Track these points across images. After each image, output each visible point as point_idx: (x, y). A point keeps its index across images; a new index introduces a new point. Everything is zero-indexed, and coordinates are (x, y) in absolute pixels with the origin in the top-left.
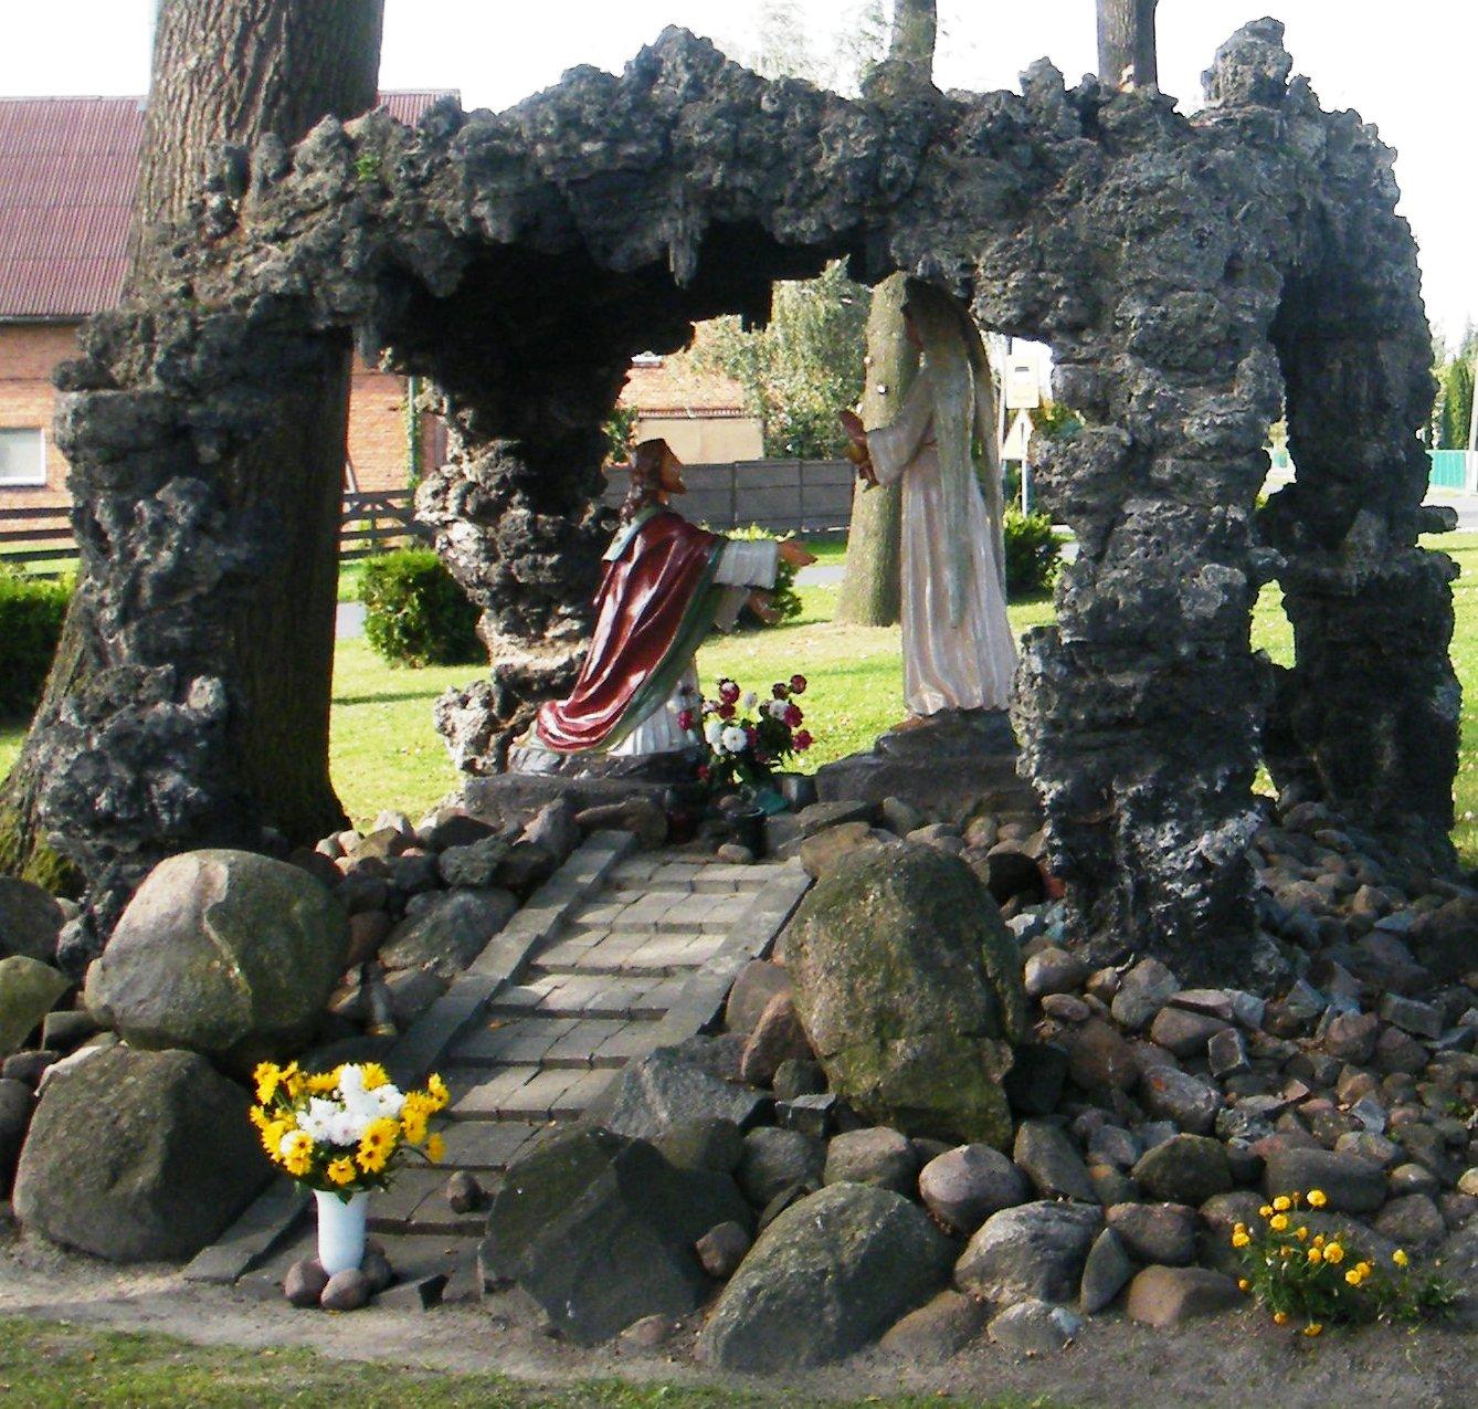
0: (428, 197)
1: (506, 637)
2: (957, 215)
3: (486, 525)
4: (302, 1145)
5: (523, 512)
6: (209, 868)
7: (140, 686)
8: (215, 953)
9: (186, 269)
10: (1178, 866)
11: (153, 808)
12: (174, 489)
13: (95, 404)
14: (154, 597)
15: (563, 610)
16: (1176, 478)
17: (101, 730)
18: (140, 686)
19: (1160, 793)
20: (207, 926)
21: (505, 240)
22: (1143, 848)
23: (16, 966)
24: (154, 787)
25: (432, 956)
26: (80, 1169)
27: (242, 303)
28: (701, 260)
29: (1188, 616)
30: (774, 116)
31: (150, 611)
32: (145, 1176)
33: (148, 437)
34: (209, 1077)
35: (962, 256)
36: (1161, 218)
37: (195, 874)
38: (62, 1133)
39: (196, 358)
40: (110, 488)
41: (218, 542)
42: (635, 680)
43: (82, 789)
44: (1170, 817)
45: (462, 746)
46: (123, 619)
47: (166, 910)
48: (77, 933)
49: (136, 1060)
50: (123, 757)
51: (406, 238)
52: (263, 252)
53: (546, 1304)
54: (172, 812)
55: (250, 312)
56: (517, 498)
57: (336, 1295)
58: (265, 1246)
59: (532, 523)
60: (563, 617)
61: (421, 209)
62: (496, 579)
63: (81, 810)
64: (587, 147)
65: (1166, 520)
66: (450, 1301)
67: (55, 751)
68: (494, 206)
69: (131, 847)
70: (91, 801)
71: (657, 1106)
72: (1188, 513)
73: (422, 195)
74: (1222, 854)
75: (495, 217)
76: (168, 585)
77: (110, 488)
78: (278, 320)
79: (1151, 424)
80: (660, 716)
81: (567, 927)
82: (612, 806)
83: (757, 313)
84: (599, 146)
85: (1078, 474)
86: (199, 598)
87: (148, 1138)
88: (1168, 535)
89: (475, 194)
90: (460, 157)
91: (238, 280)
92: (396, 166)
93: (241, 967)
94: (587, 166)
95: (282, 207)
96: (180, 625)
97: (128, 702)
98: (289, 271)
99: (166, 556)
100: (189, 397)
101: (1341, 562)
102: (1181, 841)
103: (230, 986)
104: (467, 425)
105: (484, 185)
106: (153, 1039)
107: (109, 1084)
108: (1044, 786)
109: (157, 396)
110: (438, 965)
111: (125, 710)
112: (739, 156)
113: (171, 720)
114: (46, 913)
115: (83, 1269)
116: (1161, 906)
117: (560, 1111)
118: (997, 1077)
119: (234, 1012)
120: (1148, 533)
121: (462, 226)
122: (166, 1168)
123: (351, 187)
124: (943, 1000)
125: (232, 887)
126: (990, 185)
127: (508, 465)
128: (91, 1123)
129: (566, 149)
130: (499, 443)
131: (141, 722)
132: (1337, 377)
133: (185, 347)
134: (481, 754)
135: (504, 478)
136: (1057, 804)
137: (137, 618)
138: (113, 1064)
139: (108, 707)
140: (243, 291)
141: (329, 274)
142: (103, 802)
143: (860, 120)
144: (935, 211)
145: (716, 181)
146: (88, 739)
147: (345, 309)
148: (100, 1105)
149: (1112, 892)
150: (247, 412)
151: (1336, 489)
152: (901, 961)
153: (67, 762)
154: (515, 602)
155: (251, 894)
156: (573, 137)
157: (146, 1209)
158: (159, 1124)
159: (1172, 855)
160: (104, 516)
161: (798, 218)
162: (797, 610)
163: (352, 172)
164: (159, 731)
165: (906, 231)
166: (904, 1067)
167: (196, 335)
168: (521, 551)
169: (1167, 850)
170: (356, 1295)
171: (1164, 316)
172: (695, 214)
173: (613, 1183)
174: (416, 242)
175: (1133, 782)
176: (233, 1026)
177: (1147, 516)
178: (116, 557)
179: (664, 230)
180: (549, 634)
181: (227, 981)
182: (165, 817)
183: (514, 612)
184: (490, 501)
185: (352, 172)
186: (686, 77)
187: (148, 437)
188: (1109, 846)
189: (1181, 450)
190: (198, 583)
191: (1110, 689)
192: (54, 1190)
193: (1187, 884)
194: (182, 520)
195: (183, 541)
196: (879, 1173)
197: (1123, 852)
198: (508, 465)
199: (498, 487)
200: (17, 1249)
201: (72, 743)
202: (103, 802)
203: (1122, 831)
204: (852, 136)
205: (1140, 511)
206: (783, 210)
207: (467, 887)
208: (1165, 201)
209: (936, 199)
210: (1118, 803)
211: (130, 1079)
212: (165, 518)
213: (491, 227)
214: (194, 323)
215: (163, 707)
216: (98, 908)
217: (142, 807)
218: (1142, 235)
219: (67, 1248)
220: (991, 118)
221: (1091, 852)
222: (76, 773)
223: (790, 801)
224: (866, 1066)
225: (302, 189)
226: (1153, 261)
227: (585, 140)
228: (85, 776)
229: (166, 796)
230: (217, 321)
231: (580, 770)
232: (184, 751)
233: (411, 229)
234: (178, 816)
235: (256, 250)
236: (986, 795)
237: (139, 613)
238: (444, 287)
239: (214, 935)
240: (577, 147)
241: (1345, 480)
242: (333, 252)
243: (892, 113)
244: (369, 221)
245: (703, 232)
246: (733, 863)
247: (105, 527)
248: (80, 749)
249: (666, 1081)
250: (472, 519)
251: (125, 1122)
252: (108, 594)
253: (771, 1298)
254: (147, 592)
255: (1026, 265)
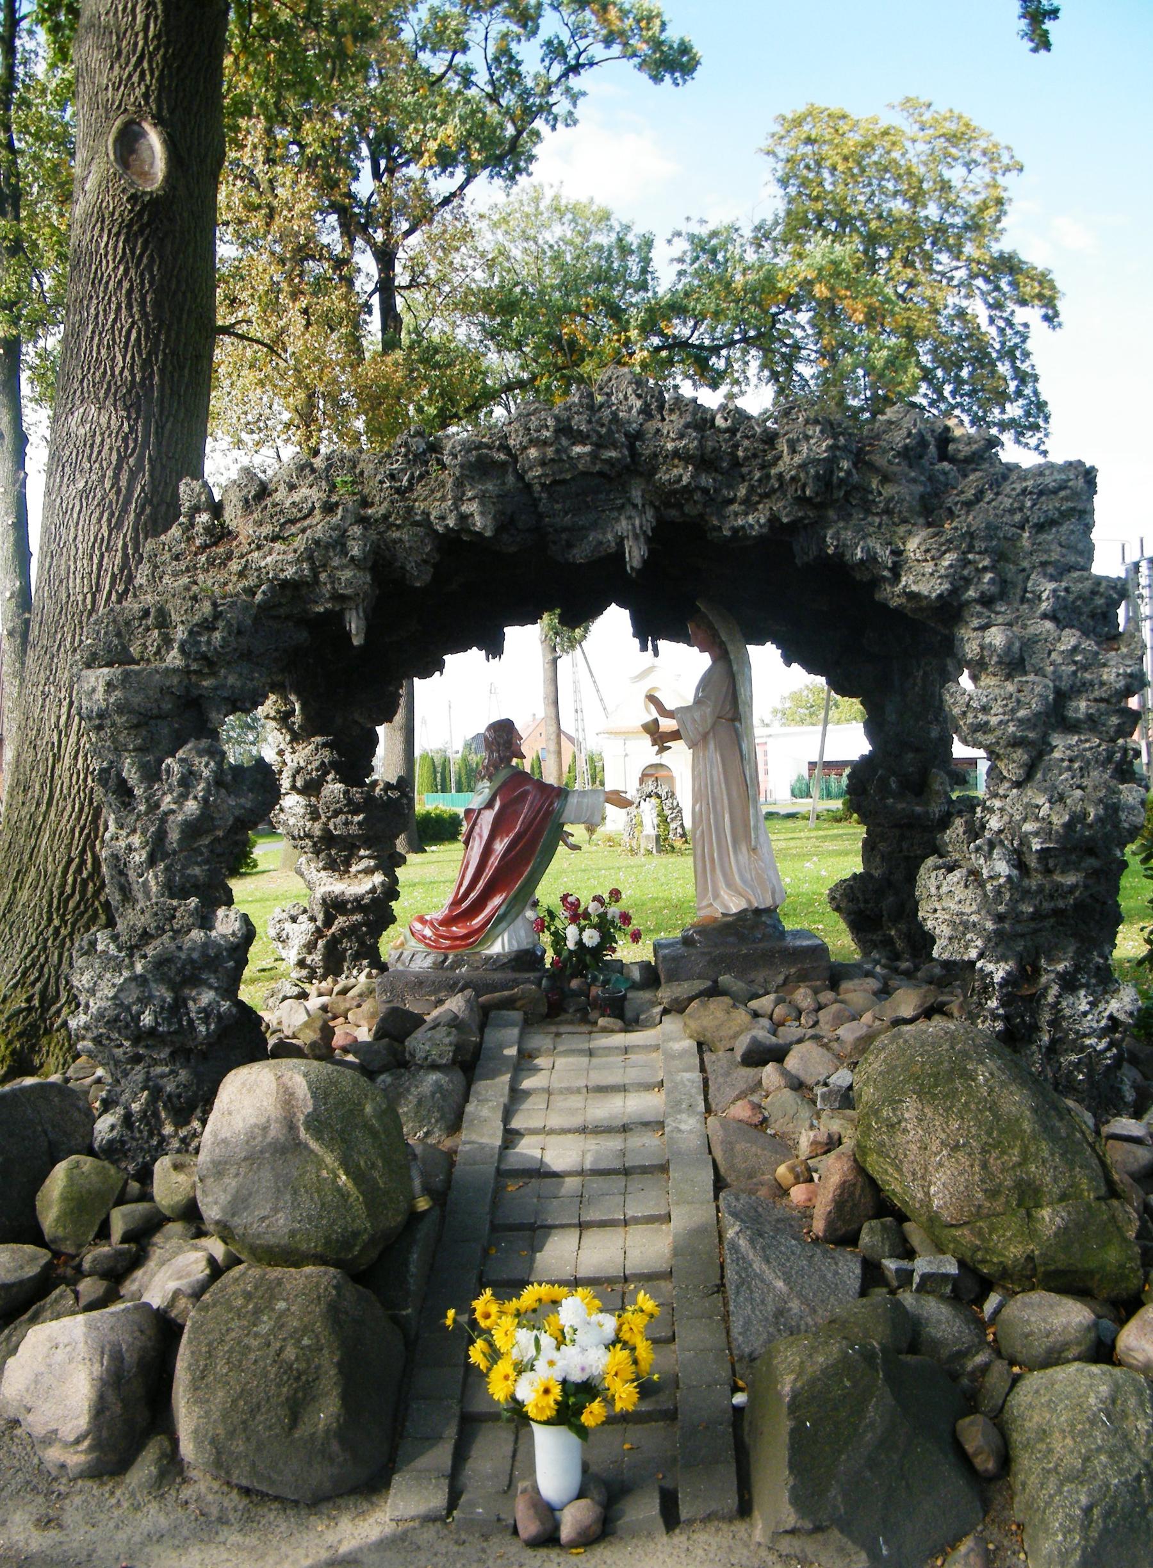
0: (415, 500)
1: (323, 873)
2: (888, 512)
3: (309, 796)
4: (547, 1391)
5: (340, 786)
6: (285, 1079)
7: (174, 917)
8: (320, 1163)
9: (188, 570)
10: (1095, 1025)
11: (191, 1022)
12: (195, 748)
13: (127, 675)
14: (181, 841)
15: (362, 852)
16: (1090, 717)
17: (145, 956)
18: (174, 917)
19: (1078, 968)
20: (303, 1134)
21: (488, 534)
22: (1068, 1012)
23: (77, 1165)
24: (191, 1003)
25: (421, 1128)
26: (254, 1411)
27: (251, 591)
28: (651, 551)
29: (1126, 825)
30: (727, 430)
31: (175, 852)
32: (326, 1413)
33: (167, 706)
34: (352, 1291)
35: (890, 544)
36: (1061, 513)
37: (274, 1085)
38: (222, 1368)
39: (217, 635)
40: (134, 750)
41: (229, 794)
42: (497, 900)
43: (128, 1009)
44: (1082, 986)
45: (296, 948)
46: (152, 861)
47: (253, 1121)
48: (113, 1127)
49: (279, 1282)
50: (163, 979)
51: (396, 535)
52: (266, 549)
53: (863, 1547)
54: (208, 1025)
55: (259, 597)
56: (330, 777)
57: (579, 1534)
58: (449, 1463)
59: (346, 792)
60: (363, 857)
61: (410, 510)
62: (318, 833)
63: (127, 1026)
64: (578, 449)
65: (1085, 750)
66: (690, 1522)
67: (100, 977)
68: (482, 504)
69: (164, 1054)
70: (136, 1018)
71: (769, 1275)
72: (1099, 746)
73: (409, 499)
74: (1131, 1014)
75: (482, 513)
76: (192, 829)
77: (134, 750)
78: (280, 605)
79: (1075, 673)
80: (519, 922)
81: (516, 1096)
82: (506, 993)
83: (494, 648)
84: (588, 449)
85: (1021, 713)
86: (217, 840)
87: (318, 1367)
88: (1088, 763)
89: (464, 494)
90: (455, 462)
91: (241, 574)
92: (379, 477)
93: (347, 1174)
94: (574, 467)
95: (272, 517)
96: (199, 864)
97: (164, 932)
98: (298, 561)
99: (191, 806)
100: (206, 670)
101: (927, 803)
102: (1093, 1004)
103: (343, 1195)
104: (296, 727)
105: (473, 487)
106: (287, 1256)
107: (257, 1312)
108: (990, 967)
109: (176, 671)
110: (427, 1134)
111: (165, 938)
112: (704, 462)
113: (205, 945)
114: (79, 1109)
115: (270, 1514)
116: (1074, 1058)
117: (634, 1275)
118: (1132, 1234)
119: (353, 1221)
120: (1071, 761)
121: (451, 523)
122: (346, 1398)
123: (335, 498)
124: (1072, 1170)
125: (314, 1096)
126: (913, 487)
127: (326, 755)
128: (252, 1356)
129: (557, 451)
130: (319, 739)
131: (180, 948)
132: (919, 681)
133: (207, 626)
134: (310, 953)
135: (323, 763)
136: (1005, 983)
137: (162, 860)
138: (256, 1288)
139: (146, 936)
140: (251, 581)
141: (336, 562)
142: (147, 1019)
143: (818, 429)
144: (867, 507)
145: (685, 480)
146: (132, 965)
147: (348, 592)
148: (256, 1335)
149: (1034, 1047)
150: (250, 685)
151: (910, 755)
152: (1034, 1138)
153: (114, 985)
154: (329, 848)
155: (331, 1100)
156: (564, 442)
157: (335, 1447)
158: (326, 1352)
159: (1090, 1017)
160: (130, 772)
161: (746, 514)
162: (255, 866)
163: (333, 487)
164: (195, 955)
165: (841, 524)
166: (1056, 1234)
167: (217, 615)
168: (337, 813)
169: (1085, 1014)
170: (596, 1529)
171: (1067, 590)
172: (650, 513)
173: (890, 1400)
174: (405, 537)
175: (1059, 961)
176: (356, 1234)
177: (1070, 747)
178: (142, 808)
179: (623, 526)
180: (353, 869)
181: (339, 1189)
182: (202, 1028)
183: (329, 855)
184: (312, 779)
185: (333, 487)
186: (638, 404)
187: (167, 706)
188: (1035, 1014)
189: (1096, 694)
190: (215, 828)
191: (1058, 886)
192: (231, 1434)
193: (1100, 1038)
194: (206, 773)
195: (207, 790)
196: (1079, 1344)
197: (1047, 1016)
198: (326, 755)
199: (317, 770)
200: (187, 1492)
201: (118, 969)
202: (147, 1019)
203: (1050, 999)
204: (812, 441)
205: (1062, 745)
206: (735, 507)
207: (434, 1067)
208: (1066, 499)
209: (871, 497)
210: (1044, 979)
211: (281, 1305)
212: (191, 773)
213: (478, 522)
214: (215, 605)
215: (197, 935)
216: (136, 1107)
217: (180, 1021)
218: (1040, 528)
219: (246, 1492)
220: (909, 434)
221: (1022, 1017)
222: (121, 995)
223: (634, 982)
224: (1013, 1235)
225: (290, 501)
226: (1054, 546)
227: (574, 444)
228: (129, 998)
229: (204, 1010)
230: (234, 603)
231: (460, 966)
232: (215, 972)
233: (398, 527)
234: (213, 1027)
235: (259, 548)
236: (793, 971)
237: (165, 855)
238: (420, 578)
239: (313, 1145)
240: (566, 450)
241: (917, 750)
242: (339, 543)
243: (840, 425)
244: (363, 521)
245: (653, 529)
246: (612, 1031)
247: (131, 783)
248: (126, 974)
249: (763, 1249)
250: (300, 792)
251: (290, 1353)
252: (136, 840)
253: (1107, 1515)
254: (174, 836)
255: (957, 548)
